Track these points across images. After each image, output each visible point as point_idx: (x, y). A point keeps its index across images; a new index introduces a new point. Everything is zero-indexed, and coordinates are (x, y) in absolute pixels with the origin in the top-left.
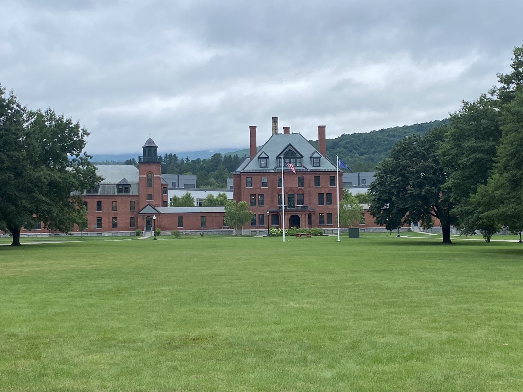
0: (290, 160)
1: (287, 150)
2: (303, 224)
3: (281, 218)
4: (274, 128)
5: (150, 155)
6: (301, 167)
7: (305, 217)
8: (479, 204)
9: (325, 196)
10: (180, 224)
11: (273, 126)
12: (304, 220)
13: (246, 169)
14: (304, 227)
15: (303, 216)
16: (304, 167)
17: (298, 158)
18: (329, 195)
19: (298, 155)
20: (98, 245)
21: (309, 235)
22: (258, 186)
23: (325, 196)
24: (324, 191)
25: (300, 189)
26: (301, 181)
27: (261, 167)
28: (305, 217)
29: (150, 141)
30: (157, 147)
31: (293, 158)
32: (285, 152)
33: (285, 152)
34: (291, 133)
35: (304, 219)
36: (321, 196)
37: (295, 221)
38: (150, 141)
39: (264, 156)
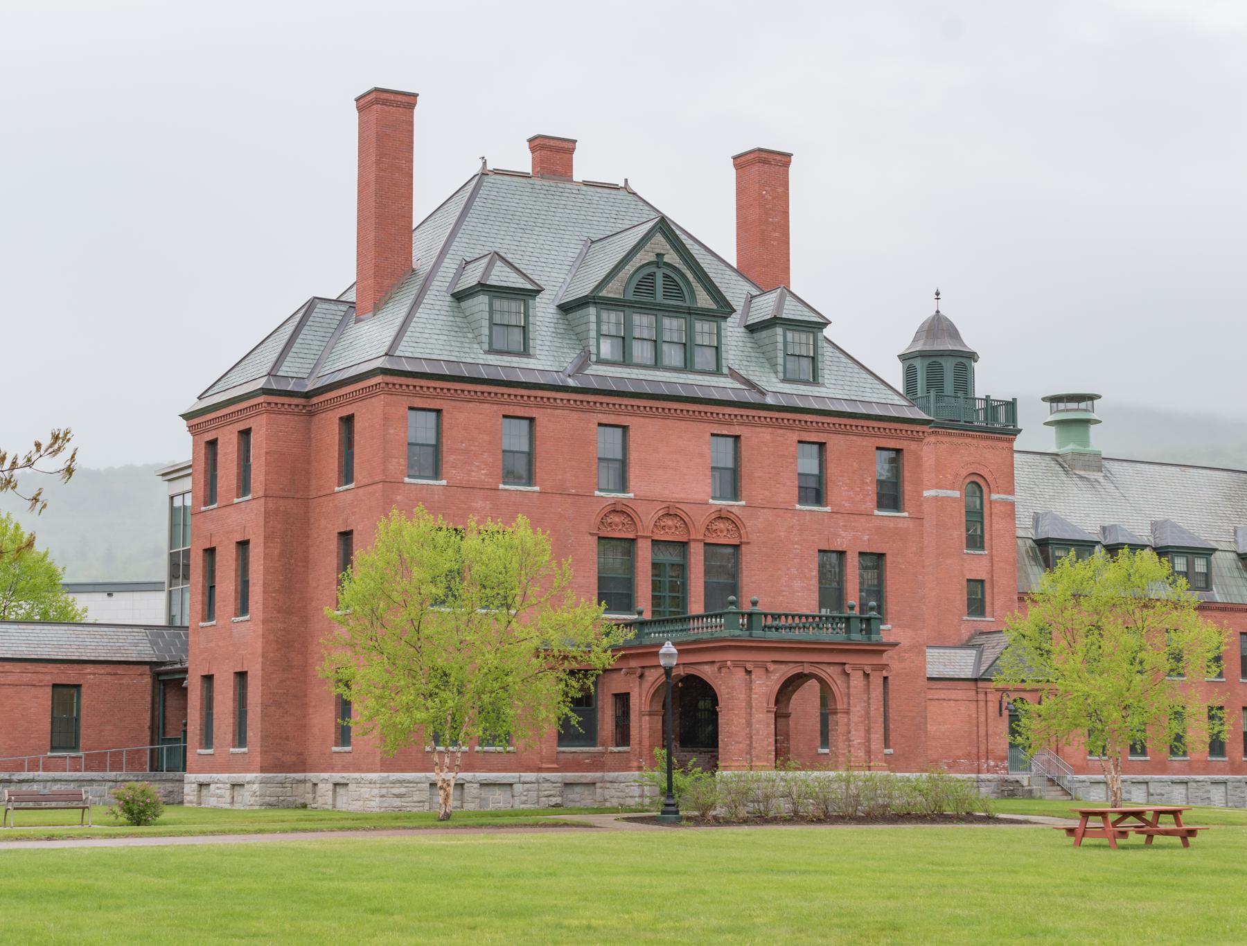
5: (935, 381)
6: (718, 372)
8: (1099, 628)
9: (853, 562)
12: (857, 710)
14: (745, 764)
15: (857, 680)
16: (733, 374)
17: (705, 314)
19: (704, 300)
20: (566, 825)
22: (480, 474)
23: (853, 562)
24: (852, 538)
25: (722, 516)
28: (868, 690)
29: (938, 326)
30: (972, 356)
31: (674, 311)
32: (630, 268)
33: (630, 268)
34: (578, 176)
35: (745, 700)
38: (938, 326)
39: (501, 276)
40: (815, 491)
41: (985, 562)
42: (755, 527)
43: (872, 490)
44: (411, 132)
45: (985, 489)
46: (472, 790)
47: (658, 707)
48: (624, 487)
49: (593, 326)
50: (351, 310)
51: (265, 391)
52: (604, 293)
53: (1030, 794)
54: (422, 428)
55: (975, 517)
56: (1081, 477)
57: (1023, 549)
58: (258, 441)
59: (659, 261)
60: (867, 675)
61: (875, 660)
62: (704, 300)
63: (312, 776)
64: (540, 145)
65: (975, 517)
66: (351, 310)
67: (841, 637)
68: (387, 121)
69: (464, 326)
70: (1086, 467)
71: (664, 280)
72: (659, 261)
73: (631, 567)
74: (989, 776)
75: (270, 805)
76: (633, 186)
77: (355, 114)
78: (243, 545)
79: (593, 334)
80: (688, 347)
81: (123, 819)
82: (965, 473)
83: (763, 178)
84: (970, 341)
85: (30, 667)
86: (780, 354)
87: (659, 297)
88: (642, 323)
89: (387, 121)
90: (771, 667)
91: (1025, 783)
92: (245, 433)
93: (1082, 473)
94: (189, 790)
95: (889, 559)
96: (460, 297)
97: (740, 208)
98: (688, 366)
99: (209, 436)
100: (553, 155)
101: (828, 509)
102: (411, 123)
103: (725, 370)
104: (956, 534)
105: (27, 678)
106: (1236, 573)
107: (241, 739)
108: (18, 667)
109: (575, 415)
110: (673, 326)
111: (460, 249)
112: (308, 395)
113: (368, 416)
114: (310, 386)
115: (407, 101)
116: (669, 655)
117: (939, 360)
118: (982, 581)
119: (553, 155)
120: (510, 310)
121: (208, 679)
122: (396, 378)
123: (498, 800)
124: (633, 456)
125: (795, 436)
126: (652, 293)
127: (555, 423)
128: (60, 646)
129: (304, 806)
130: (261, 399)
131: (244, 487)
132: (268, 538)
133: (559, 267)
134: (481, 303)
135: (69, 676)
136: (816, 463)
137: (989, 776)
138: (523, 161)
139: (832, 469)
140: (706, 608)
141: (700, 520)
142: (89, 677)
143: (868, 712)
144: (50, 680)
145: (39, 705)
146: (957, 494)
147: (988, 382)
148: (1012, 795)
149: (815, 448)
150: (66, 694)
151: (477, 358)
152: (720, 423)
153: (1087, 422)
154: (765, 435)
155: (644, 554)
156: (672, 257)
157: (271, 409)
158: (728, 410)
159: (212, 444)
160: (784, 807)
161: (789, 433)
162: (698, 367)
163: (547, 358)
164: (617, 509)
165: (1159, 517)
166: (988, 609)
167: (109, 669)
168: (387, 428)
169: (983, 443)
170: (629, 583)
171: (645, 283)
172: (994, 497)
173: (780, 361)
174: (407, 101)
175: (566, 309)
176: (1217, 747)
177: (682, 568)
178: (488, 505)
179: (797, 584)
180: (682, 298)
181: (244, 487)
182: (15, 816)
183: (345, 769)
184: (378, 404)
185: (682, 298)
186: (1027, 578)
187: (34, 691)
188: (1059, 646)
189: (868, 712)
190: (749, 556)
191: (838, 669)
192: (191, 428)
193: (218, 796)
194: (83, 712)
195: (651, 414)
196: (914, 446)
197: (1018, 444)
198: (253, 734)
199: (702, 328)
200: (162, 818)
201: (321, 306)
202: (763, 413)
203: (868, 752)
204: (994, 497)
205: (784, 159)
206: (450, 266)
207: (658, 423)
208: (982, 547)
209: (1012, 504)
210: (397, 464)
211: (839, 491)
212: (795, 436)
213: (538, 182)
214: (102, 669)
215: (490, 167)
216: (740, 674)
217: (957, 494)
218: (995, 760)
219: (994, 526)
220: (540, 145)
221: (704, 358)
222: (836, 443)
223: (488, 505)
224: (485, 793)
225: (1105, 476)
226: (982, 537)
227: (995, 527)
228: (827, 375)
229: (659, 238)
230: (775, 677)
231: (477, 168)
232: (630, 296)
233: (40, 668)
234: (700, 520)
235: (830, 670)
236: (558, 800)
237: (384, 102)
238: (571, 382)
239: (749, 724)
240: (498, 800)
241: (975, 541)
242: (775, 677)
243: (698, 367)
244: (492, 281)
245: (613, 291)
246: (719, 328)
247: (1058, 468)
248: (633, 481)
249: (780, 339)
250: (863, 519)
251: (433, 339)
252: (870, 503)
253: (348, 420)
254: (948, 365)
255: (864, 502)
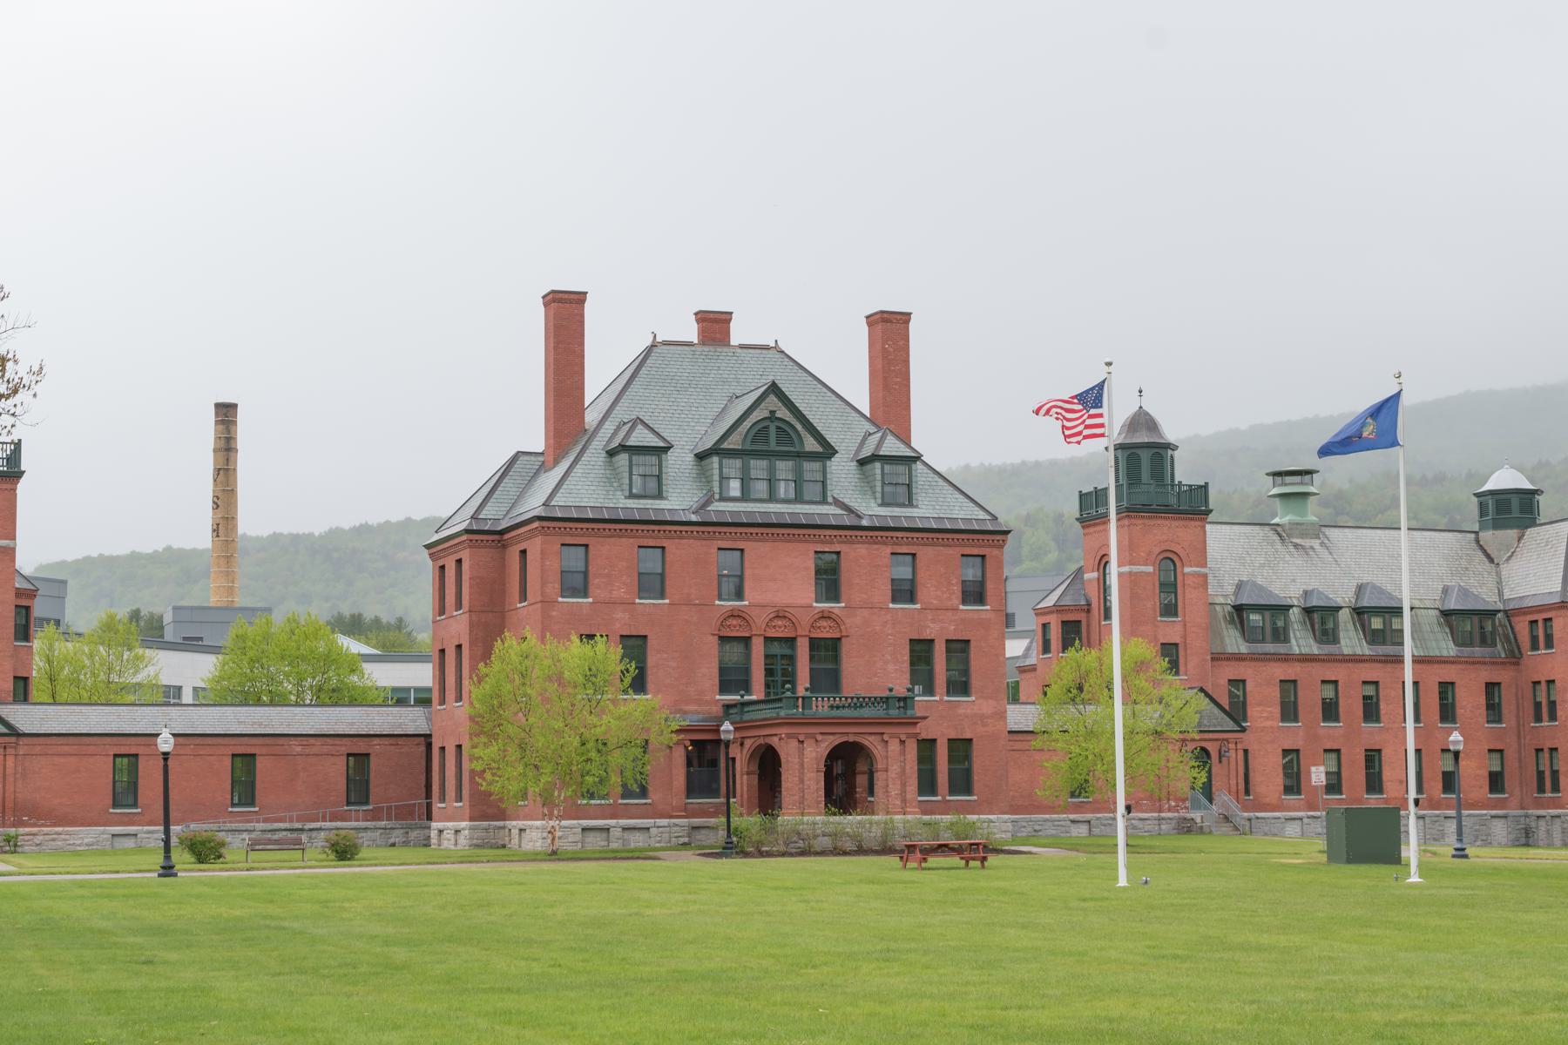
0: (772, 470)
1: (757, 415)
2: (894, 791)
3: (56, 882)
4: (222, 444)
6: (824, 501)
7: (903, 752)
9: (939, 652)
10: (245, 790)
11: (218, 438)
12: (894, 769)
13: (559, 500)
14: (896, 808)
15: (894, 746)
17: (813, 456)
18: (959, 648)
19: (811, 445)
21: (912, 852)
22: (620, 592)
24: (938, 630)
25: (825, 616)
26: (829, 580)
27: (632, 496)
28: (903, 752)
30: (1168, 446)
32: (747, 424)
33: (747, 424)
34: (734, 341)
35: (894, 763)
36: (921, 651)
37: (846, 778)
39: (641, 437)
40: (905, 592)
41: (1179, 628)
42: (854, 624)
43: (957, 589)
44: (582, 322)
45: (1178, 564)
46: (616, 833)
47: (755, 767)
48: (739, 595)
49: (716, 472)
50: (544, 462)
51: (467, 531)
52: (725, 445)
53: (1201, 831)
54: (574, 559)
55: (1169, 587)
56: (1296, 546)
57: (1221, 615)
58: (465, 566)
59: (772, 416)
60: (902, 742)
61: (911, 730)
62: (811, 445)
63: (508, 823)
64: (704, 318)
65: (1169, 587)
66: (544, 462)
67: (882, 713)
68: (565, 313)
69: (612, 477)
70: (1303, 535)
71: (778, 432)
72: (772, 416)
73: (748, 655)
74: (1170, 815)
75: (477, 846)
76: (782, 346)
77: (542, 308)
78: (459, 647)
79: (716, 477)
80: (798, 482)
81: (332, 857)
82: (1157, 550)
83: (889, 331)
84: (1170, 434)
85: (329, 740)
86: (879, 484)
87: (773, 446)
88: (758, 467)
89: (565, 313)
90: (819, 737)
91: (1198, 820)
92: (459, 561)
93: (1298, 541)
94: (434, 834)
95: (972, 644)
96: (611, 454)
97: (871, 358)
98: (799, 499)
99: (441, 563)
100: (714, 325)
101: (918, 606)
102: (582, 316)
103: (830, 500)
104: (1149, 605)
105: (325, 749)
106: (1437, 629)
107: (459, 798)
108: (319, 741)
109: (698, 543)
110: (784, 468)
111: (621, 414)
112: (502, 533)
113: (535, 547)
114: (503, 525)
115: (579, 299)
116: (728, 732)
117: (1139, 451)
118: (1176, 645)
119: (714, 325)
120: (647, 463)
121: (443, 749)
122: (548, 522)
123: (637, 840)
124: (748, 573)
125: (889, 550)
126: (767, 442)
127: (680, 550)
128: (353, 724)
129: (504, 846)
130: (465, 537)
131: (459, 606)
132: (472, 644)
133: (690, 424)
134: (623, 459)
135: (361, 747)
136: (910, 569)
137: (1170, 815)
138: (691, 333)
139: (922, 574)
140: (768, 694)
141: (805, 620)
142: (375, 747)
143: (903, 772)
144: (344, 750)
145: (336, 771)
146: (1150, 569)
147: (1185, 472)
148: (1189, 831)
149: (909, 558)
150: (360, 760)
151: (621, 503)
152: (822, 542)
153: (1305, 495)
154: (862, 550)
155: (758, 648)
156: (783, 413)
157: (472, 545)
158: (828, 532)
159: (443, 567)
160: (826, 842)
161: (883, 548)
162: (807, 498)
163: (680, 499)
164: (735, 614)
165: (1366, 579)
166: (1182, 669)
167: (392, 741)
168: (544, 559)
169: (1176, 523)
170: (747, 671)
171: (760, 433)
172: (1187, 570)
173: (879, 489)
174: (579, 299)
175: (701, 457)
176: (1496, 781)
177: (791, 659)
178: (627, 616)
179: (891, 667)
180: (792, 444)
181: (459, 606)
182: (253, 855)
183: (526, 818)
184: (538, 540)
185: (792, 444)
186: (1222, 639)
187: (332, 759)
188: (1161, 708)
189: (903, 772)
190: (846, 647)
191: (878, 738)
192: (431, 555)
193: (448, 841)
194: (372, 775)
195: (762, 539)
196: (995, 552)
197: (1211, 518)
198: (466, 793)
199: (811, 468)
200: (360, 855)
201: (523, 458)
202: (859, 533)
203: (904, 801)
204: (1187, 570)
205: (905, 318)
206: (609, 427)
207: (768, 545)
208: (1176, 615)
209: (1205, 576)
210: (553, 587)
211: (929, 591)
212: (889, 550)
213: (699, 349)
214: (386, 741)
215: (659, 339)
216: (794, 743)
217: (1150, 569)
218: (1176, 800)
219: (1188, 597)
220: (704, 318)
221: (812, 491)
222: (926, 553)
223: (627, 616)
224: (627, 835)
225: (1322, 544)
226: (1176, 605)
227: (1188, 596)
228: (920, 497)
229: (772, 398)
230: (824, 745)
231: (648, 342)
232: (748, 447)
233: (337, 741)
234: (805, 620)
235: (872, 738)
236: (686, 840)
237: (560, 301)
238: (694, 518)
239: (802, 781)
240: (637, 840)
241: (1170, 610)
242: (824, 745)
243: (807, 498)
244: (631, 442)
245: (734, 442)
246: (824, 468)
247: (1276, 538)
248: (747, 591)
249: (878, 471)
250: (950, 613)
251: (587, 487)
252: (956, 601)
253: (524, 552)
254: (1145, 456)
255: (949, 599)
